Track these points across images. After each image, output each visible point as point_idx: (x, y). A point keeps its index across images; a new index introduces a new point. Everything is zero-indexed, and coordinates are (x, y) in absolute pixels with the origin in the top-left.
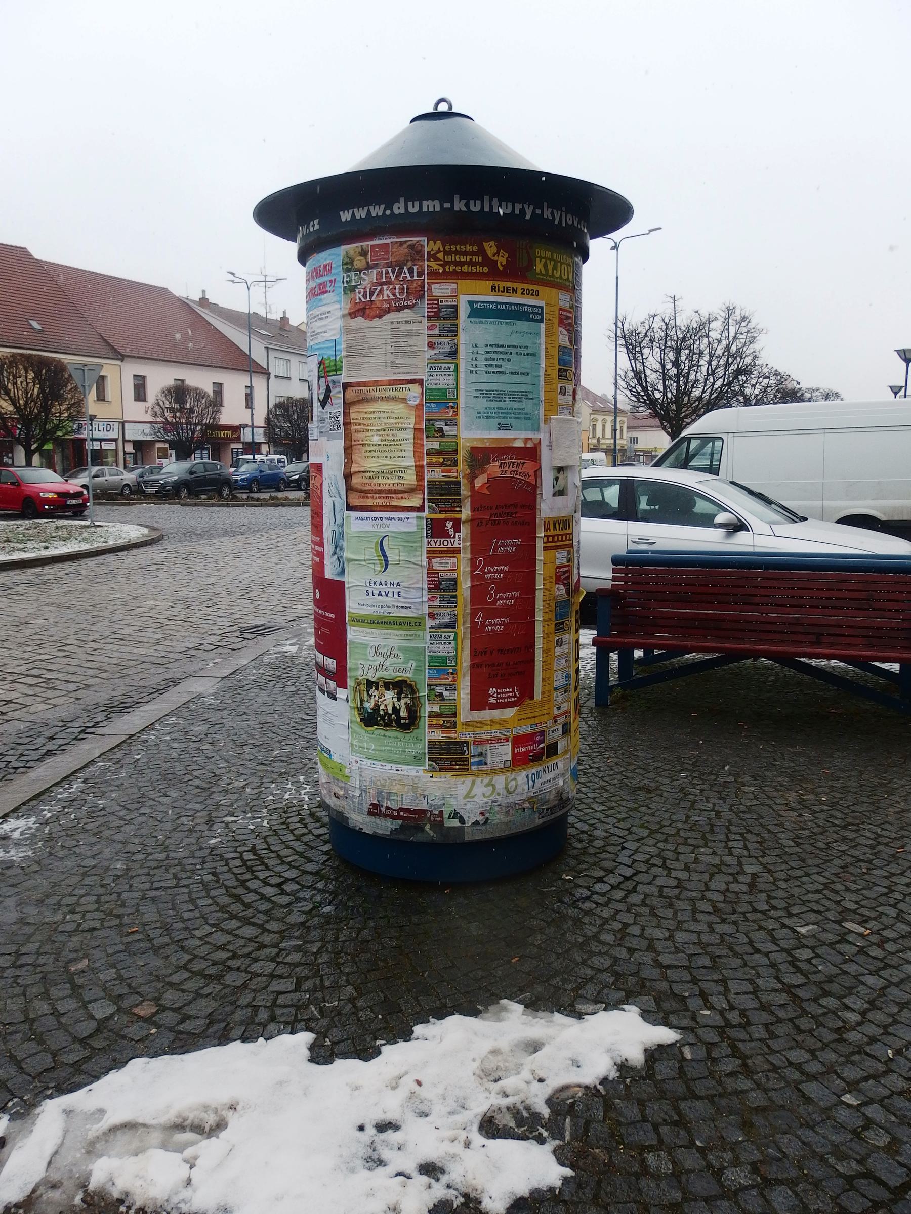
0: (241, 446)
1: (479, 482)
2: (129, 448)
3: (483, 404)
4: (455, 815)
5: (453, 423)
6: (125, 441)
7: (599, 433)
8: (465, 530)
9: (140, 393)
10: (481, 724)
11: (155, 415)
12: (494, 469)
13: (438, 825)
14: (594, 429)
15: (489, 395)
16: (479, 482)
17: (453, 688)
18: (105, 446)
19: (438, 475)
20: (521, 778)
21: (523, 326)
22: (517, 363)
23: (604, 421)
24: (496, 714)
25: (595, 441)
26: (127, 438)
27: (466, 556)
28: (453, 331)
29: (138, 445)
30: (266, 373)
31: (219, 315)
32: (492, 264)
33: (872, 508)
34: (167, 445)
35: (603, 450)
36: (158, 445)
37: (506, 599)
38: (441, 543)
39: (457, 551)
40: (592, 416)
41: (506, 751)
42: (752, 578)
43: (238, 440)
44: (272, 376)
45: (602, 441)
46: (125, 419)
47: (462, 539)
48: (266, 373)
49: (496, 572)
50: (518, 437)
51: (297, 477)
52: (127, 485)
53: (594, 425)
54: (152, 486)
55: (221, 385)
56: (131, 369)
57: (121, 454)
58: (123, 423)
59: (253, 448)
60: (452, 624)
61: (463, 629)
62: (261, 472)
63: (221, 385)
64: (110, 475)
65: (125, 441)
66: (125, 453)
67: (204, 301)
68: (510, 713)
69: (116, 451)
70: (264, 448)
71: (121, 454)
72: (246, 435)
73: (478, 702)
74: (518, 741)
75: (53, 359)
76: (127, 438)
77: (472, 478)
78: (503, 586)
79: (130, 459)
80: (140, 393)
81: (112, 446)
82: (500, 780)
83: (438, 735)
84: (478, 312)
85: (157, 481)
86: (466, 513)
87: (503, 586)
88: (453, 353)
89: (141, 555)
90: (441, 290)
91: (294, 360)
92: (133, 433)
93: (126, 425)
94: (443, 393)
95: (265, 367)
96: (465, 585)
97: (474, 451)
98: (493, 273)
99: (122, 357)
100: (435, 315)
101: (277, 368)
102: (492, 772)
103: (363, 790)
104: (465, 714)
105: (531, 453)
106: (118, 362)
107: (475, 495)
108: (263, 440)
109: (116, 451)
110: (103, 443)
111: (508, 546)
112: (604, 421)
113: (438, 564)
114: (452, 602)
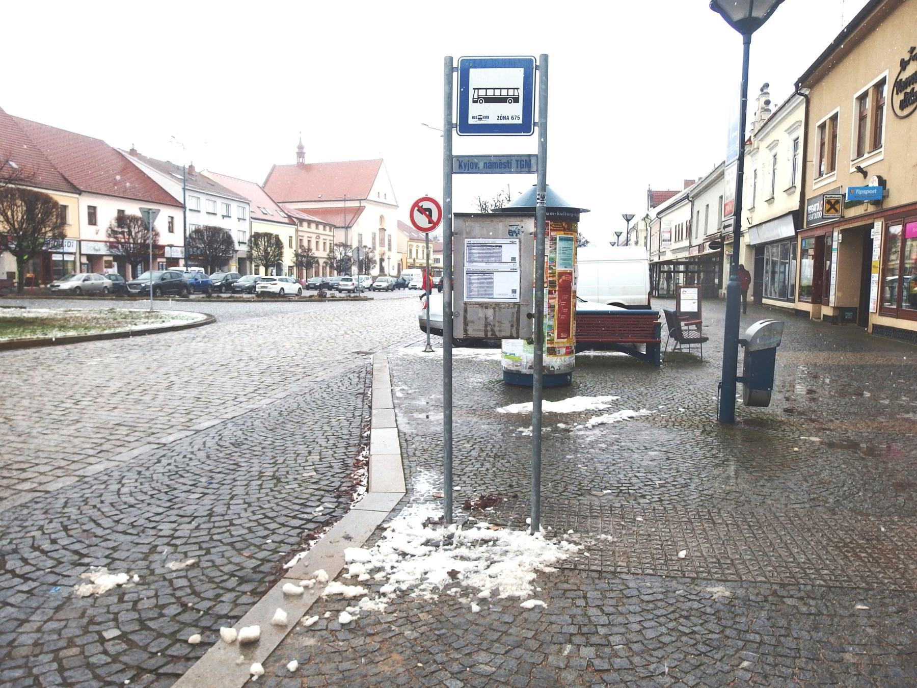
0: (164, 260)
1: (561, 281)
2: (84, 260)
3: (562, 261)
4: (553, 367)
5: (555, 266)
6: (81, 255)
7: (414, 256)
8: (557, 293)
9: (92, 217)
10: (559, 343)
11: (109, 236)
12: (564, 277)
13: (548, 369)
14: (411, 252)
15: (562, 259)
16: (561, 281)
17: (553, 333)
18: (67, 258)
19: (551, 279)
20: (567, 358)
21: (570, 242)
22: (569, 252)
23: (417, 246)
24: (562, 340)
25: (412, 261)
26: (83, 252)
27: (557, 299)
28: (555, 244)
29: (90, 257)
30: (182, 206)
31: (144, 162)
32: (564, 227)
33: (623, 300)
34: (111, 258)
35: (418, 267)
36: (105, 258)
37: (565, 310)
38: (551, 296)
39: (555, 298)
40: (409, 243)
41: (564, 351)
42: (70, 586)
43: (163, 255)
44: (187, 210)
45: (417, 261)
46: (82, 238)
47: (556, 295)
48: (182, 206)
49: (563, 303)
50: (568, 270)
51: (219, 284)
52: (106, 287)
53: (411, 250)
54: (135, 288)
55: (95, 208)
56: (86, 201)
57: (78, 264)
58: (80, 242)
59: (173, 262)
60: (553, 316)
61: (556, 317)
62: (196, 279)
63: (95, 208)
64: (96, 280)
65: (81, 255)
66: (81, 264)
67: (133, 152)
68: (566, 340)
69: (74, 262)
70: (182, 262)
71: (78, 264)
72: (168, 252)
73: (559, 337)
74: (567, 348)
75: (42, 193)
76: (83, 252)
77: (559, 280)
78: (565, 307)
79: (84, 267)
80: (92, 217)
81: (71, 258)
82: (563, 358)
83: (549, 346)
84: (561, 239)
85: (140, 284)
86: (557, 289)
87: (565, 307)
88: (555, 249)
89: (203, 330)
90: (553, 234)
91: (203, 198)
92: (87, 249)
93: (82, 243)
94: (553, 259)
95: (182, 202)
96: (557, 307)
97: (559, 273)
98: (564, 230)
99: (79, 192)
100: (551, 240)
101: (191, 204)
102: (562, 356)
103: (527, 362)
104: (556, 340)
105: (571, 274)
106: (77, 196)
107: (559, 284)
108: (180, 256)
109: (74, 262)
110: (65, 256)
111: (566, 297)
112: (417, 246)
113: (550, 301)
114: (553, 311)
